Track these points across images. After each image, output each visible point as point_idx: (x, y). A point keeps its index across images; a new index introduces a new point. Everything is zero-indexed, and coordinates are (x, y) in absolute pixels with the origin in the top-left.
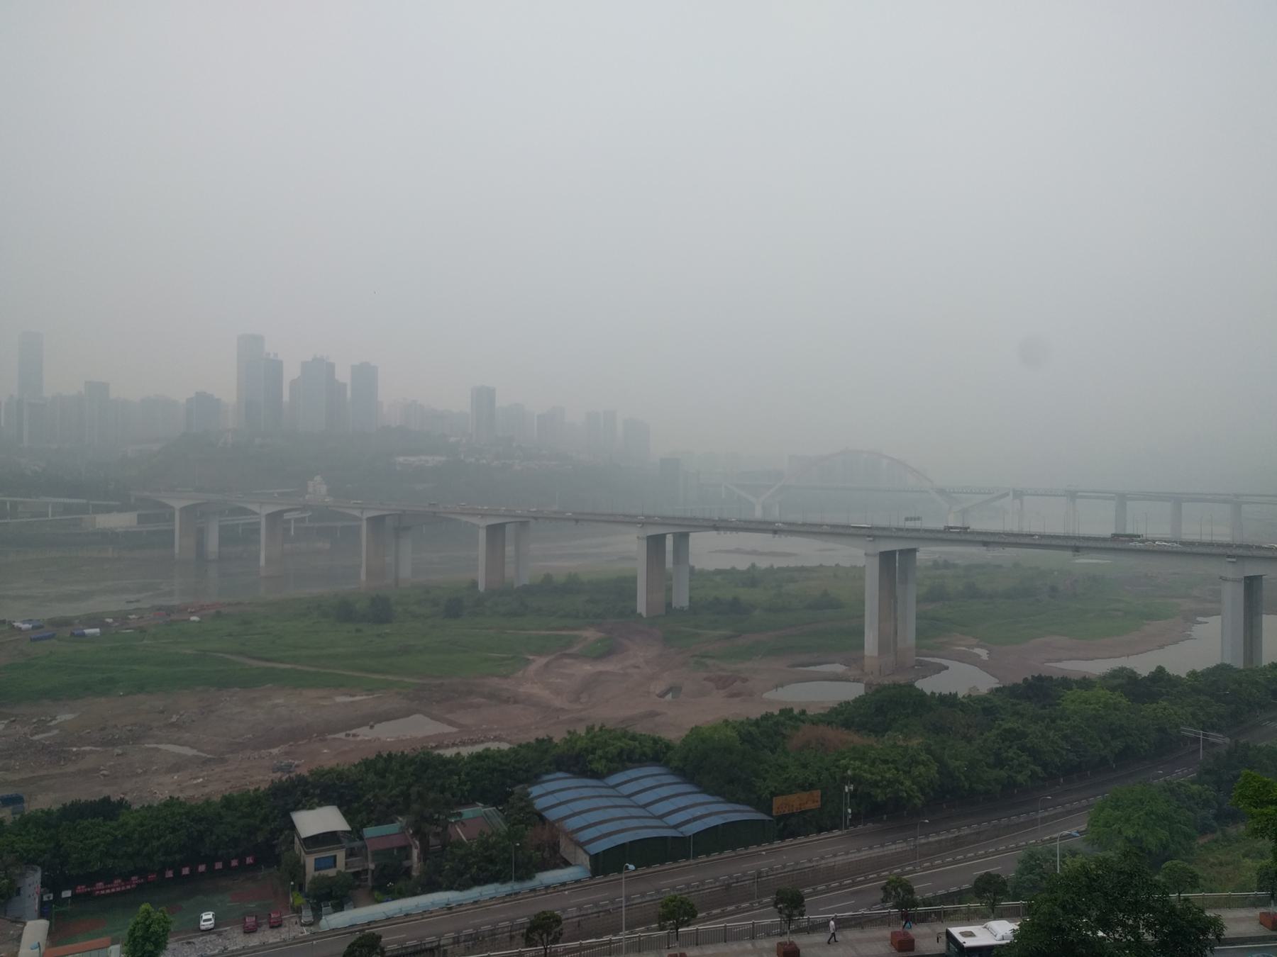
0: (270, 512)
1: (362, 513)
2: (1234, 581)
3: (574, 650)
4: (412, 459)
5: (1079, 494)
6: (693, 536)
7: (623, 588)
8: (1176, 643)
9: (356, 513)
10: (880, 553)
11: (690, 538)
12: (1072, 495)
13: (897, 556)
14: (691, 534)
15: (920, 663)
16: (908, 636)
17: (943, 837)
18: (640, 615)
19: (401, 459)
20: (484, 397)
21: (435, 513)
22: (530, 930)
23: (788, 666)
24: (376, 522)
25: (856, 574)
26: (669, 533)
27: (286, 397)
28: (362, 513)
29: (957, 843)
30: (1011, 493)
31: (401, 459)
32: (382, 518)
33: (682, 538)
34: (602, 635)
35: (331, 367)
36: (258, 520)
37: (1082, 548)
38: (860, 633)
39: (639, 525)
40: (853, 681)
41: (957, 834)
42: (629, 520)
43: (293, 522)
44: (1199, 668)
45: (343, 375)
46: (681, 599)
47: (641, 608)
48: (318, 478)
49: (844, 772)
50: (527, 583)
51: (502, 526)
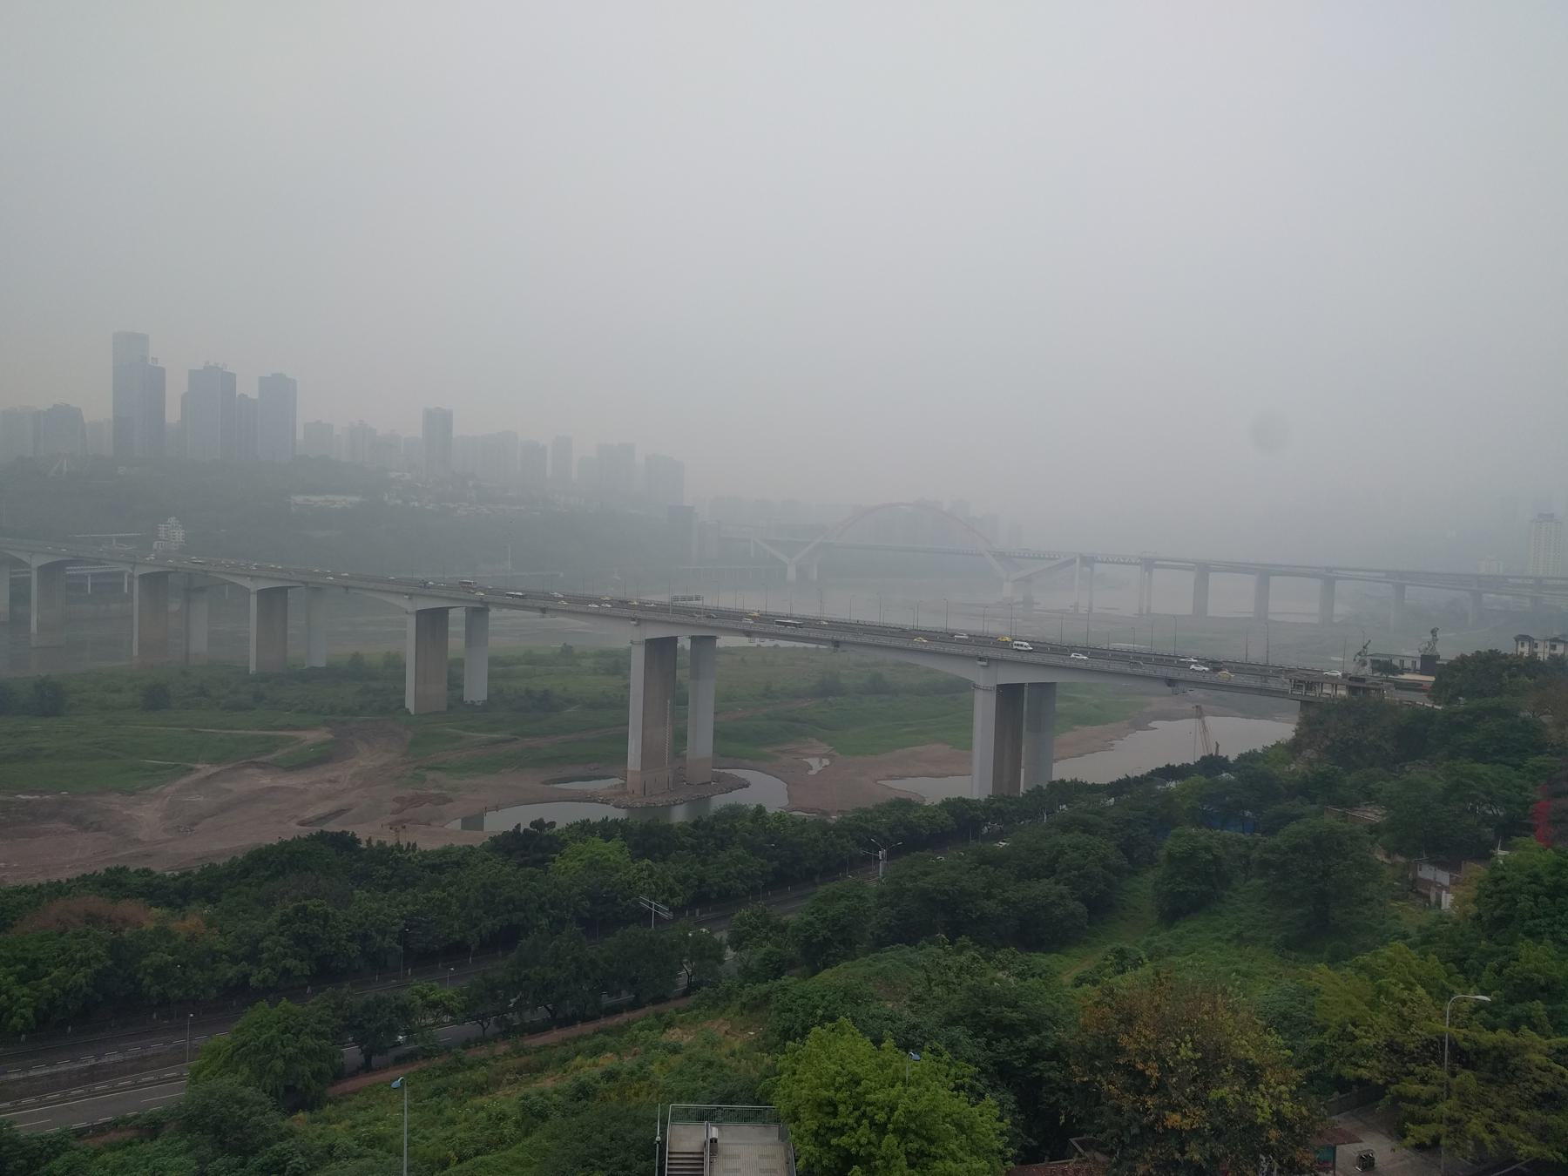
0: (43, 563)
1: (133, 569)
2: (986, 690)
4: (314, 498)
5: (1157, 563)
8: (1093, 752)
10: (646, 640)
12: (1149, 564)
15: (718, 779)
16: (701, 744)
17: (63, 1068)
18: (408, 712)
19: (299, 499)
20: (438, 421)
23: (545, 783)
25: (616, 665)
27: (173, 414)
29: (92, 1075)
30: (1078, 560)
31: (299, 499)
33: (478, 613)
34: (330, 736)
35: (230, 379)
36: (29, 575)
38: (624, 739)
39: (407, 597)
40: (602, 803)
41: (93, 1062)
43: (89, 578)
44: (952, 797)
45: (248, 387)
46: (476, 689)
47: (410, 704)
48: (172, 520)
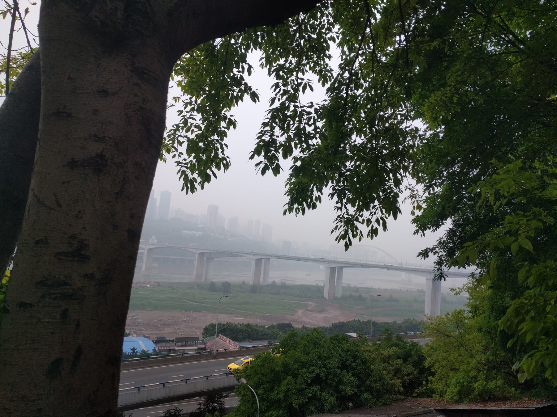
1: (196, 251)
3: (310, 308)
4: (189, 232)
6: (345, 270)
7: (319, 290)
9: (194, 251)
11: (344, 270)
13: (337, 270)
14: (344, 268)
18: (325, 298)
19: (185, 232)
21: (179, 247)
22: (337, 377)
24: (201, 255)
26: (263, 259)
28: (196, 251)
31: (185, 232)
32: (204, 253)
37: (390, 268)
42: (322, 261)
49: (470, 382)
50: (139, 252)
51: (261, 259)
